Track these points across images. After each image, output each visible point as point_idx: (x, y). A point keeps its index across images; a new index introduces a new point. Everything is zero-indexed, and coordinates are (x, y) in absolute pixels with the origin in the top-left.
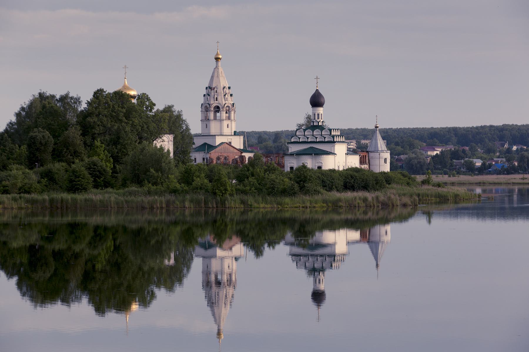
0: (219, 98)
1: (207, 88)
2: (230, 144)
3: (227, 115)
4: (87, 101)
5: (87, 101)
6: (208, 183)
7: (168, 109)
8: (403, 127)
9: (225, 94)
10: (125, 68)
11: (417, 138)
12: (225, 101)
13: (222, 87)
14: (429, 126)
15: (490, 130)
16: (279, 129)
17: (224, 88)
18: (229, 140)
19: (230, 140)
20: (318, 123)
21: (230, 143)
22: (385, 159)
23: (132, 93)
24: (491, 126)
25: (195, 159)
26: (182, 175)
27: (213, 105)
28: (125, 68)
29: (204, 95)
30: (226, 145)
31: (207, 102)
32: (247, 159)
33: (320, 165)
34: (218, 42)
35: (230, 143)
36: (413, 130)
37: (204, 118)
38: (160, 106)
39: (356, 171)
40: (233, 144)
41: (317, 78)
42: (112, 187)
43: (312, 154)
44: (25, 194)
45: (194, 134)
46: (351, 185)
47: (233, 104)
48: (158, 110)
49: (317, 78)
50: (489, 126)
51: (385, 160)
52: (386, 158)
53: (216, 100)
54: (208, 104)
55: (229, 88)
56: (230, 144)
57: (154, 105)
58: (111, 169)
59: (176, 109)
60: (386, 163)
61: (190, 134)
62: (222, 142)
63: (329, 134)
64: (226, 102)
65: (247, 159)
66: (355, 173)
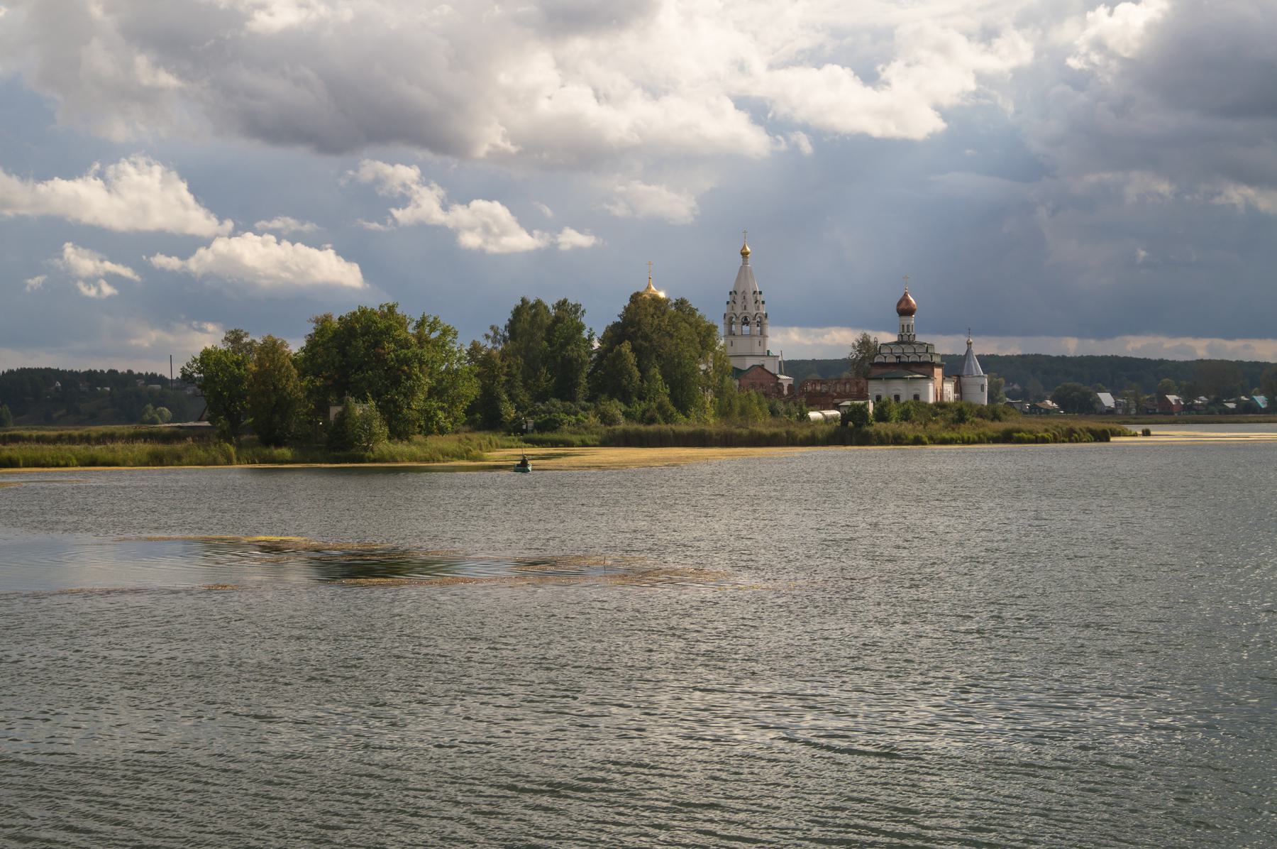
0: (748, 307)
1: (731, 293)
2: (762, 367)
3: (759, 328)
6: (598, 424)
13: (752, 292)
17: (755, 292)
19: (762, 363)
23: (9, 752)
26: (998, 398)
29: (728, 303)
32: (786, 388)
33: (917, 392)
34: (745, 232)
37: (727, 333)
40: (766, 367)
43: (881, 379)
44: (304, 344)
47: (766, 314)
51: (982, 387)
55: (760, 293)
56: (762, 367)
58: (669, 396)
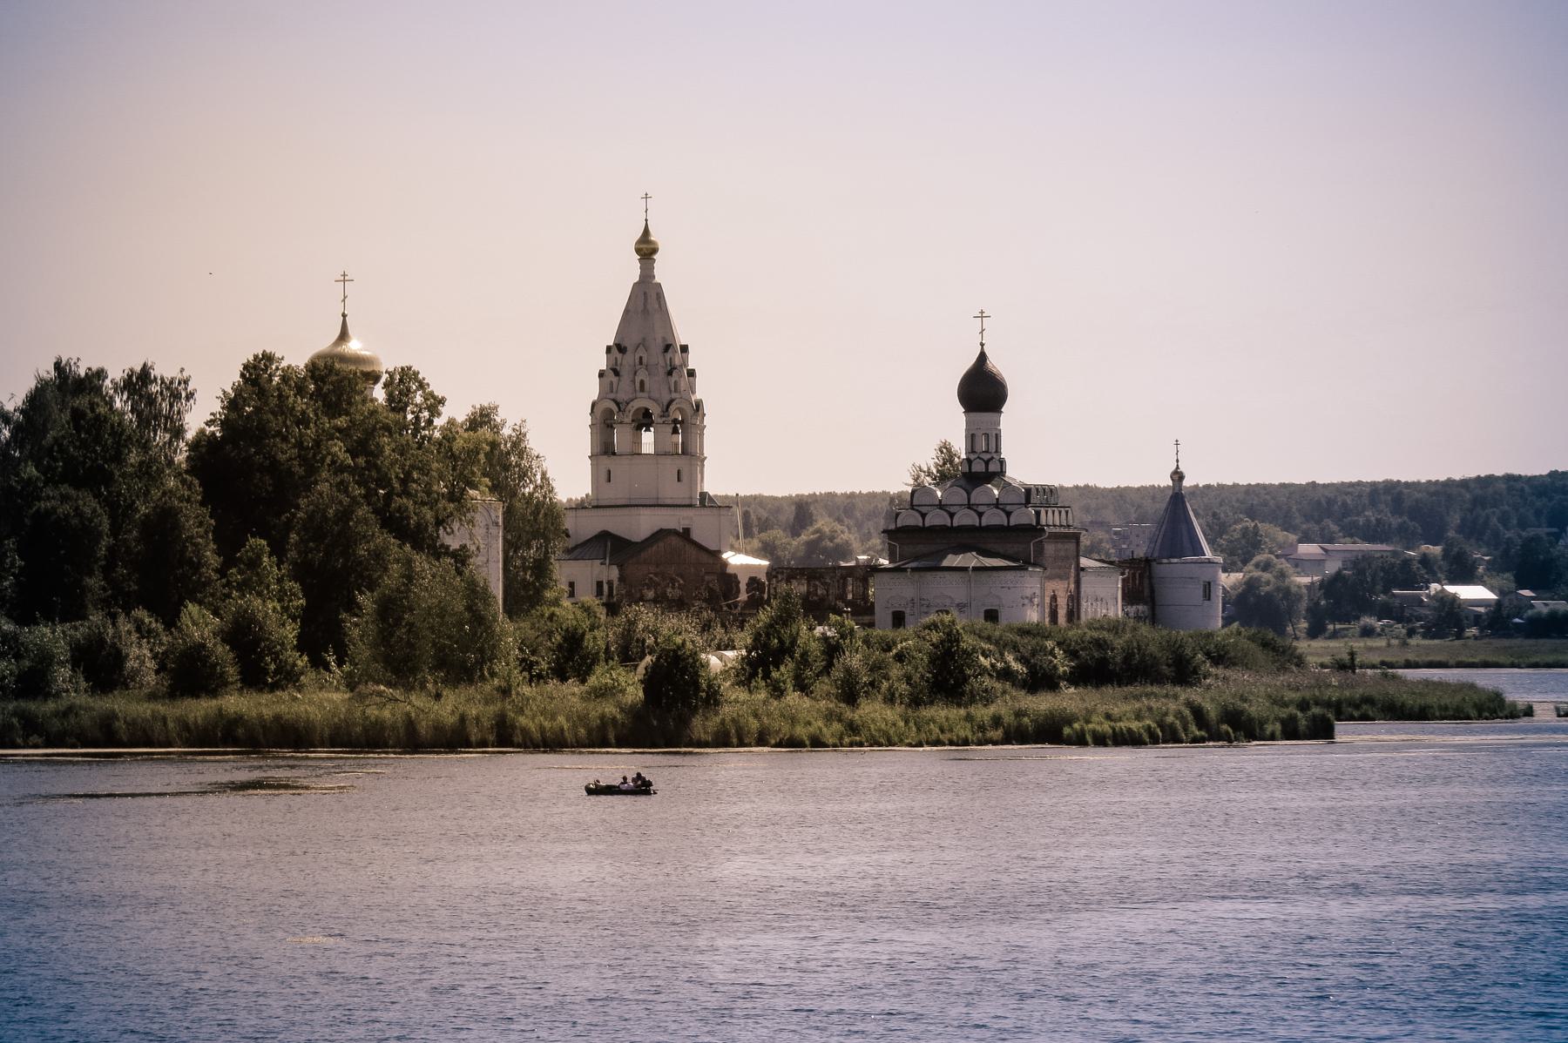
1: (609, 349)
4: (223, 391)
5: (223, 391)
7: (482, 419)
8: (1214, 483)
9: (669, 368)
10: (982, 317)
11: (1272, 518)
12: (671, 391)
14: (1301, 479)
15: (1510, 489)
16: (805, 489)
18: (682, 522)
19: (685, 524)
20: (987, 463)
21: (687, 531)
22: (1205, 586)
24: (1509, 478)
25: (572, 585)
27: (630, 405)
28: (982, 317)
30: (674, 540)
31: (612, 396)
32: (743, 587)
35: (687, 531)
36: (1250, 490)
38: (456, 411)
39: (1019, 630)
40: (695, 536)
41: (982, 316)
42: (1247, 667)
45: (570, 500)
46: (230, 679)
48: (451, 422)
49: (344, 279)
50: (1504, 476)
52: (1209, 583)
53: (676, 391)
54: (614, 400)
57: (442, 401)
59: (508, 419)
60: (1209, 599)
61: (553, 505)
62: (661, 531)
63: (1024, 502)
64: (674, 395)
65: (743, 587)
66: (1105, 634)
